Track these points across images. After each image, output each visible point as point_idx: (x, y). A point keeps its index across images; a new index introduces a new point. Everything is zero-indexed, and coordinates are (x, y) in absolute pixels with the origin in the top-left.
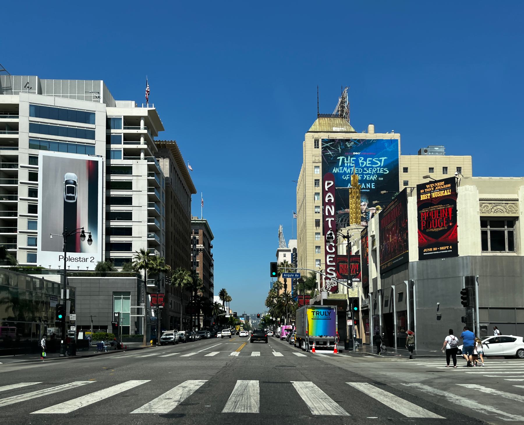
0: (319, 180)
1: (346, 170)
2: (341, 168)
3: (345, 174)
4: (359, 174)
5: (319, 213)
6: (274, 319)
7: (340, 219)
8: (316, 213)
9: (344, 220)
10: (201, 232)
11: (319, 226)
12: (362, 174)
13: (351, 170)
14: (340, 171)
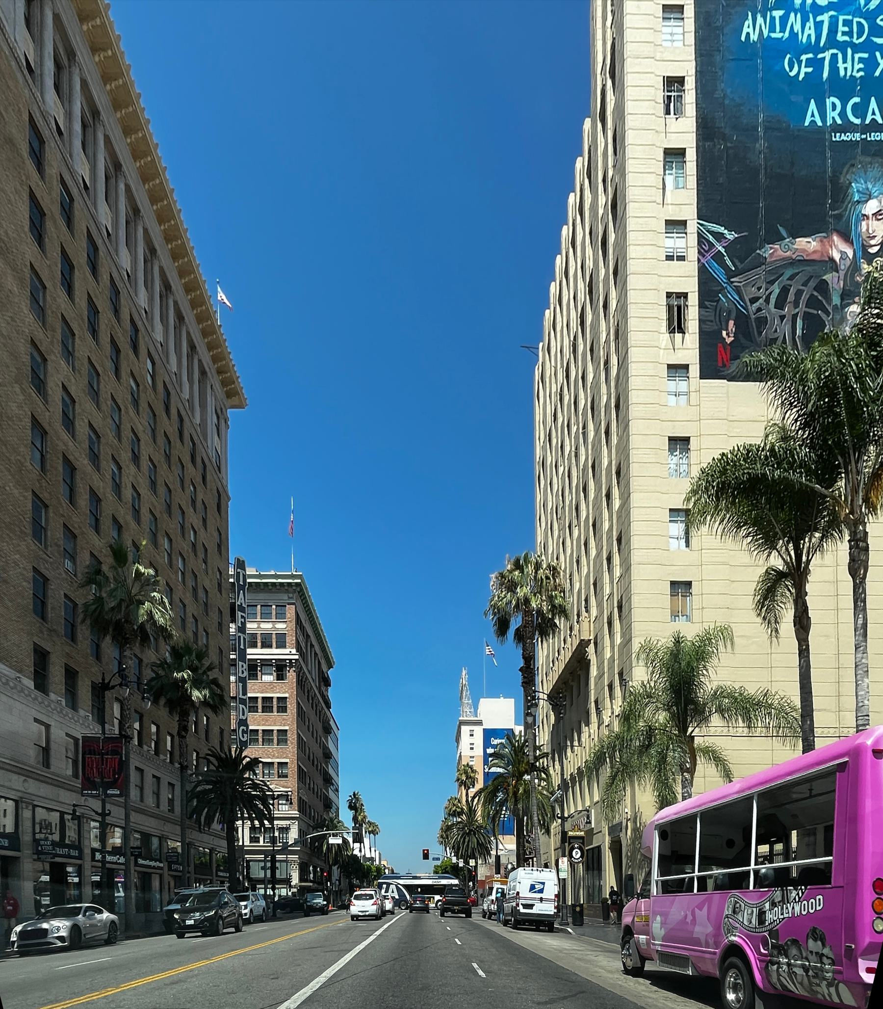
0: (685, 295)
1: (797, 28)
2: (778, 14)
3: (793, 46)
4: (856, 48)
5: (682, 258)
6: (461, 864)
7: (776, 290)
8: (669, 258)
9: (791, 297)
10: (290, 611)
11: (679, 112)
12: (868, 46)
13: (818, 26)
14: (772, 29)
